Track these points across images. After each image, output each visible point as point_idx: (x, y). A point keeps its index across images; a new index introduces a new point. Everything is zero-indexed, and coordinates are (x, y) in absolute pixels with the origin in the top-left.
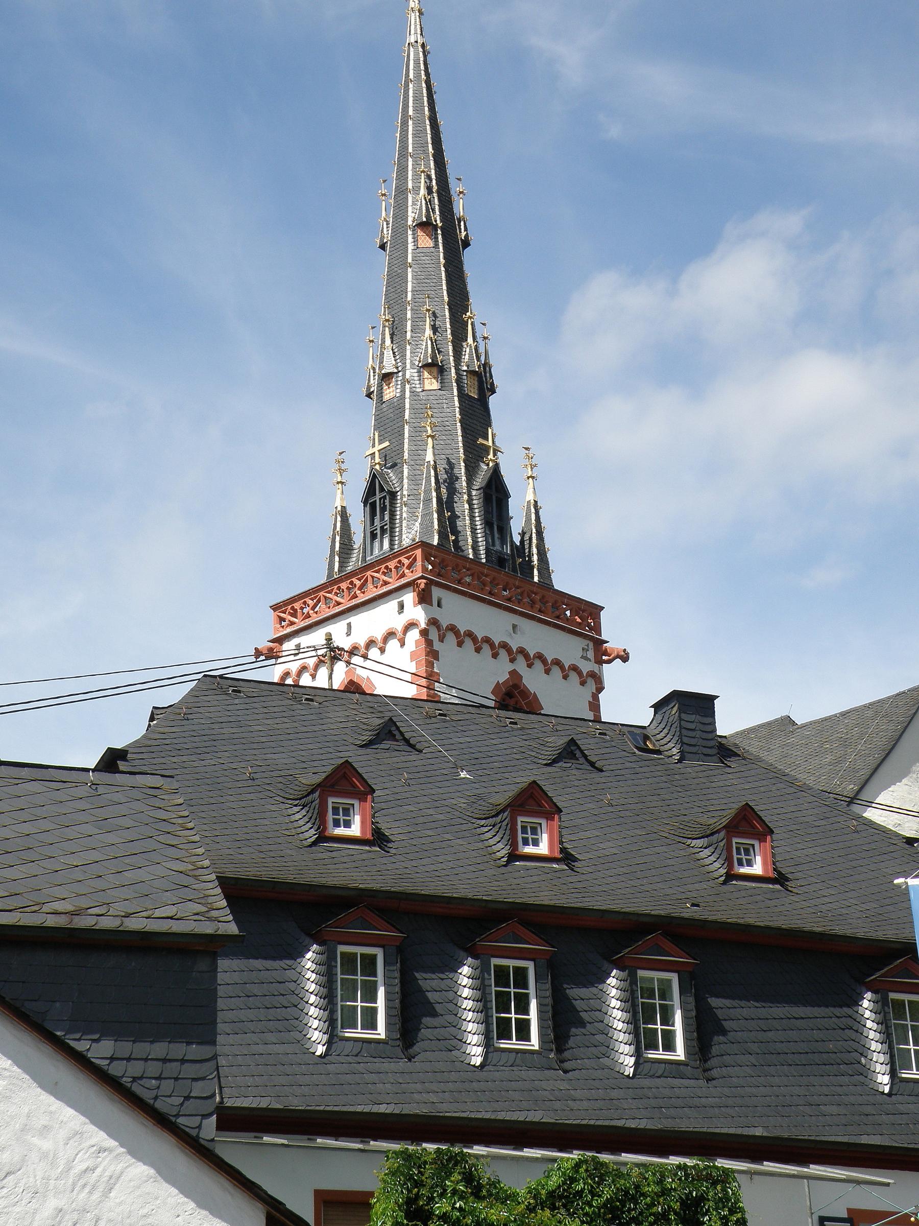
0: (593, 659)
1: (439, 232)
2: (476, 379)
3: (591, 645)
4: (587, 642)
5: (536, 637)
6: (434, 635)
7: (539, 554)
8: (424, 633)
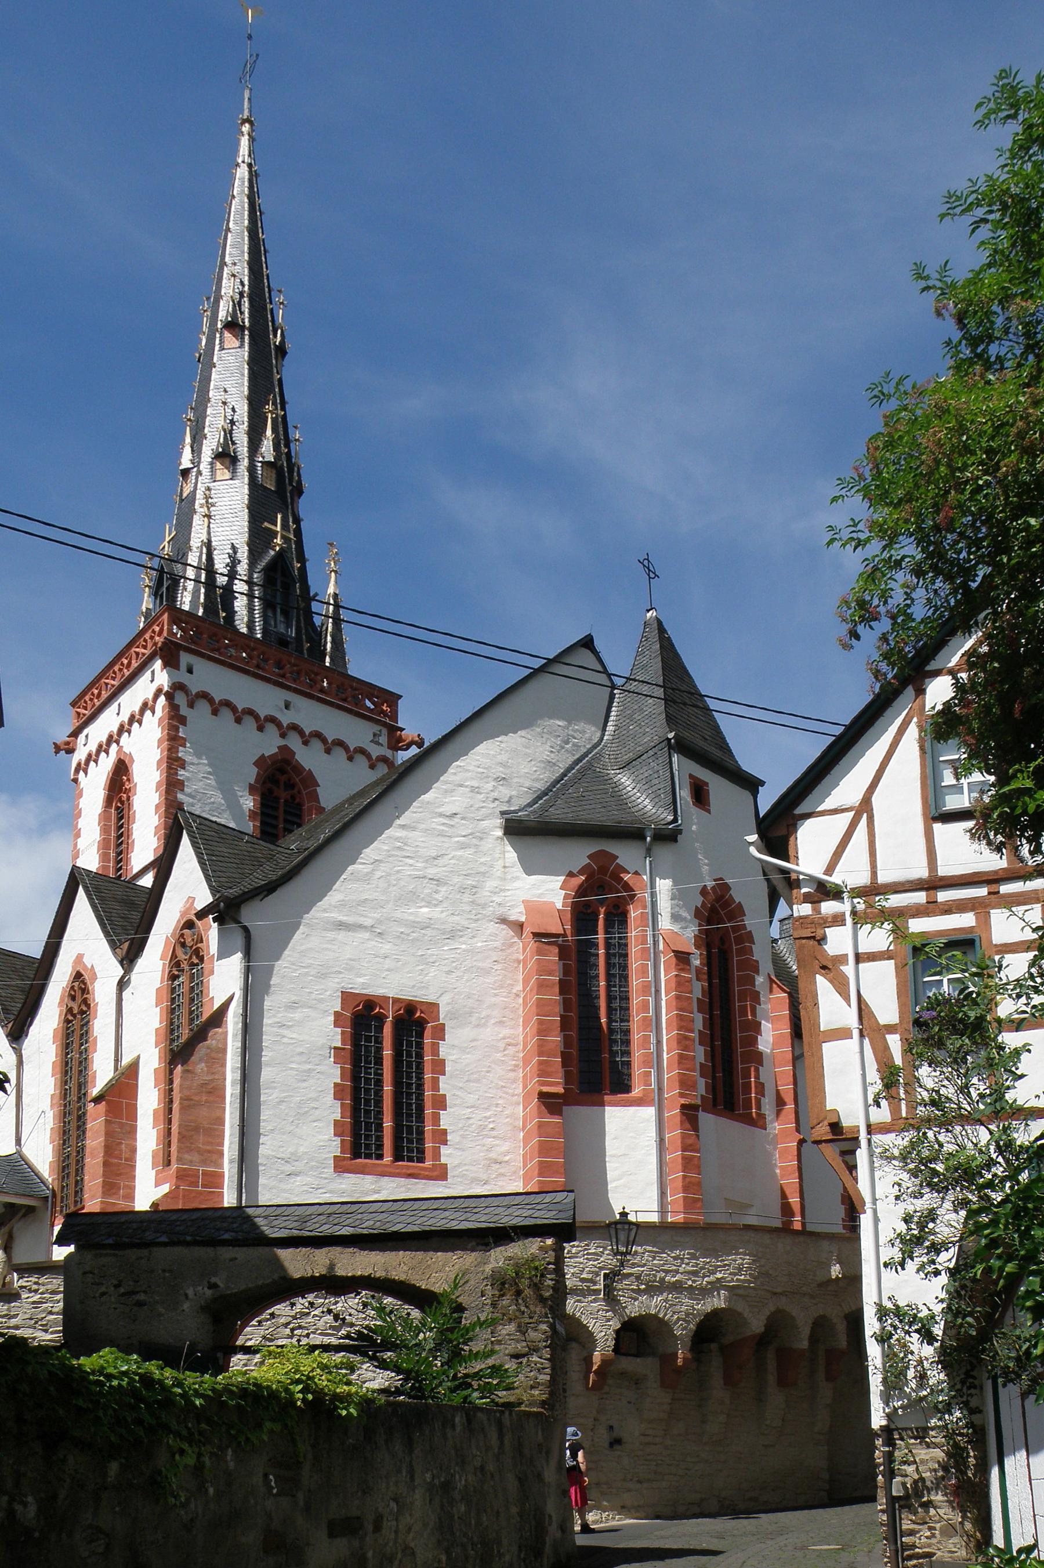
0: (386, 744)
1: (246, 332)
3: (385, 731)
4: (379, 728)
5: (310, 714)
6: (181, 699)
8: (169, 696)
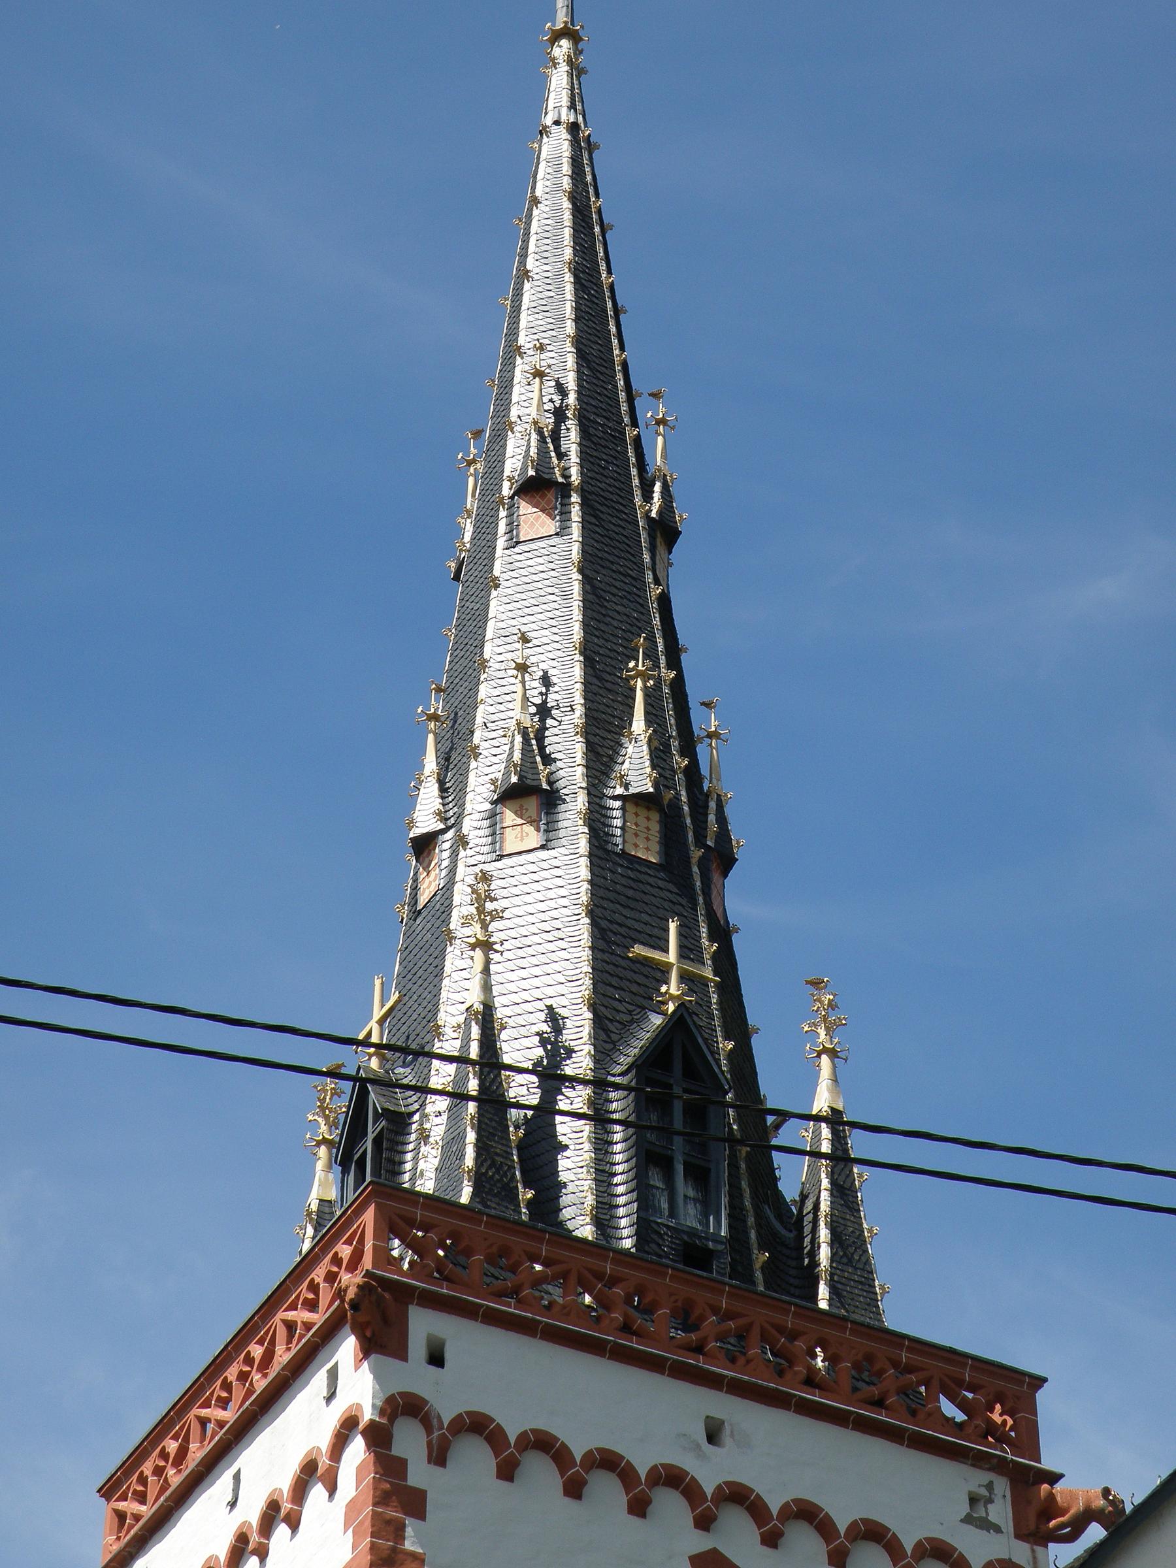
0: (1008, 1526)
1: (575, 498)
2: (655, 816)
3: (1002, 1486)
4: (984, 1477)
6: (410, 1442)
7: (836, 1240)
8: (378, 1437)
